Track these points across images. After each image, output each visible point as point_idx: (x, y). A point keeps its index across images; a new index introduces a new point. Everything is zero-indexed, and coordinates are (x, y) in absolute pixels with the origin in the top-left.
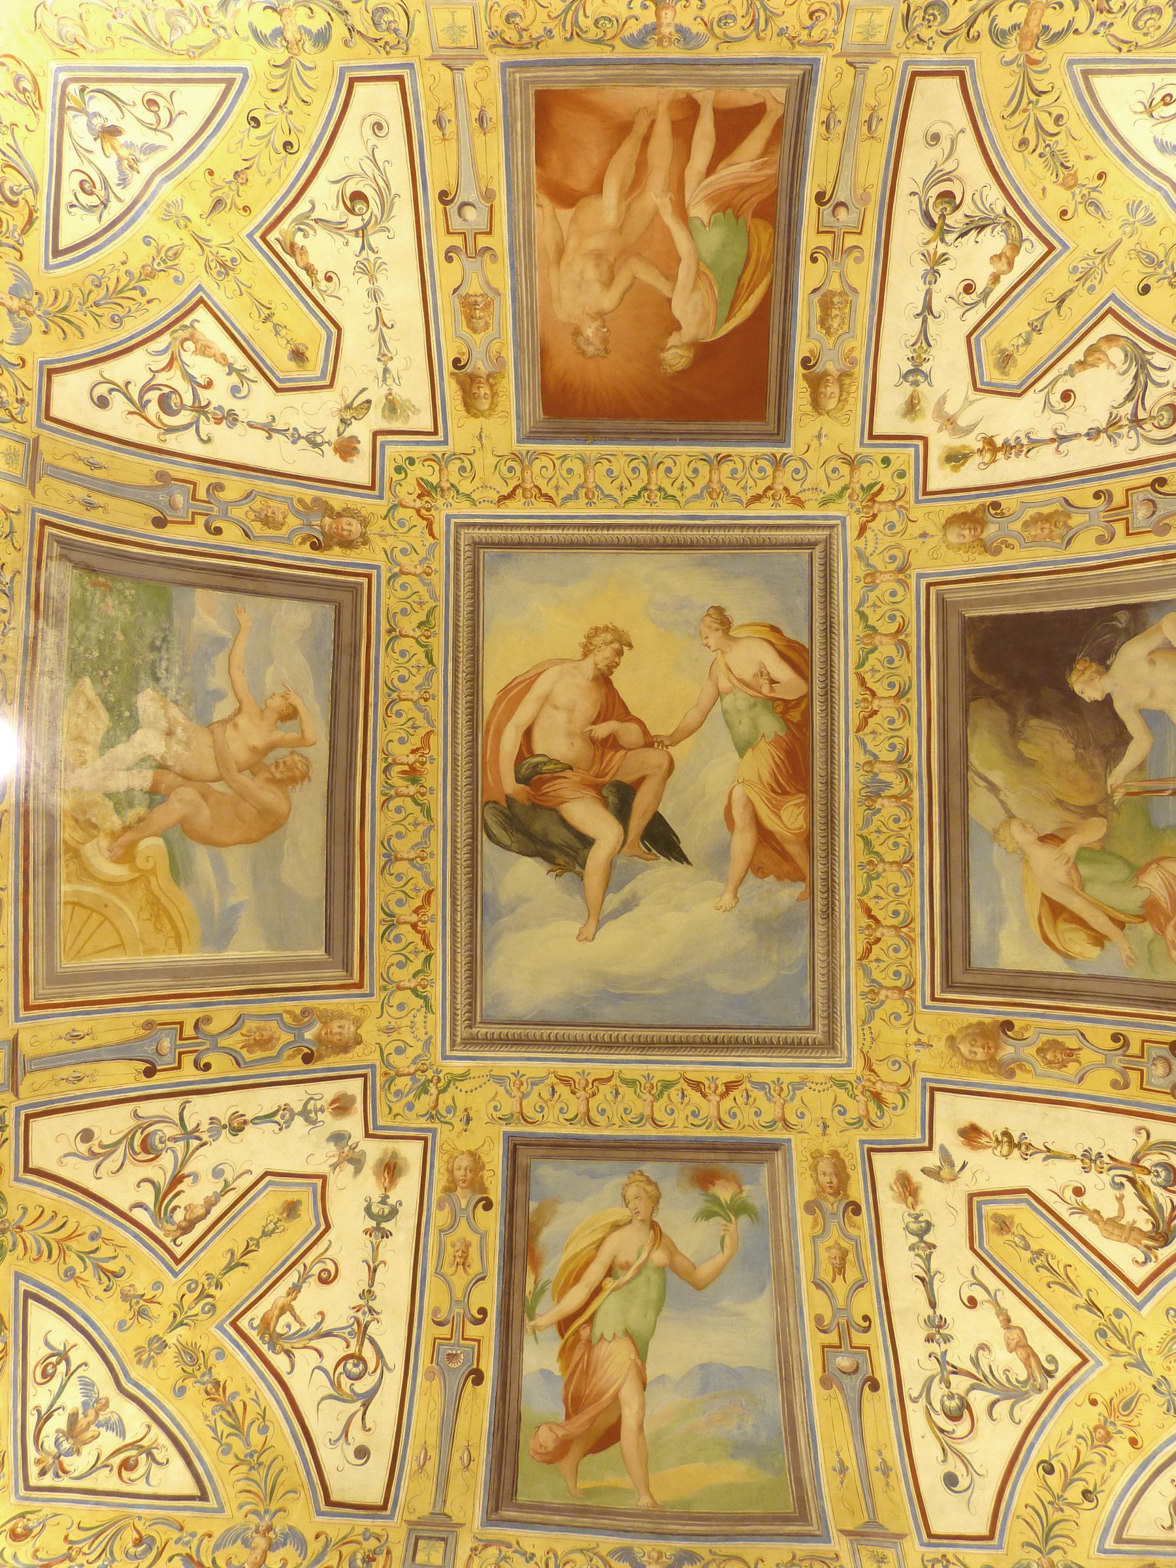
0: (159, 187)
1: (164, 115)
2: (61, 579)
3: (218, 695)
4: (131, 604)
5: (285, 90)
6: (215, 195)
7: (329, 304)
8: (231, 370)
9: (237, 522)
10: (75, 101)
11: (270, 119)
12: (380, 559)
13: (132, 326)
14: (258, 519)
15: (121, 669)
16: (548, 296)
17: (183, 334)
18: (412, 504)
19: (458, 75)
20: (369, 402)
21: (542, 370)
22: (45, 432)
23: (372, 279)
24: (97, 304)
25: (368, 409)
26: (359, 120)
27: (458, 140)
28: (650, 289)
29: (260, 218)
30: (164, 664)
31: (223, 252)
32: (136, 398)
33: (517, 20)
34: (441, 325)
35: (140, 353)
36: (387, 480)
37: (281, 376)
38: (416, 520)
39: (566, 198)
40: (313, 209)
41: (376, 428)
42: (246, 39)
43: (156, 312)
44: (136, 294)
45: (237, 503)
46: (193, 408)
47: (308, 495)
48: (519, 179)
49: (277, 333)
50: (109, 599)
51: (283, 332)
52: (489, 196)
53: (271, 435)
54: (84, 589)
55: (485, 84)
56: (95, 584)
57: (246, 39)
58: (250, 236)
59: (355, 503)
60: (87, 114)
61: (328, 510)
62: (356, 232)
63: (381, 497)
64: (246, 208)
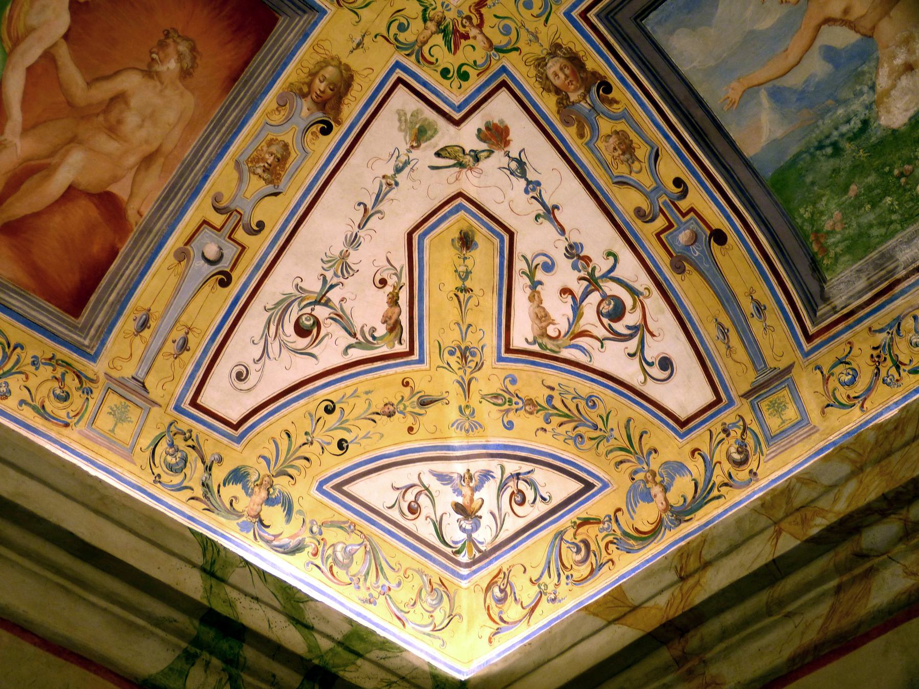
0: (462, 448)
1: (410, 496)
2: (846, 284)
3: (830, 54)
4: (814, 204)
5: (298, 454)
6: (422, 411)
7: (401, 260)
8: (535, 285)
9: (654, 173)
10: (470, 552)
11: (328, 439)
12: (558, 19)
13: (585, 388)
14: (634, 158)
15: (884, 165)
16: (191, 126)
17: (550, 344)
18: (480, 37)
19: (141, 376)
20: (438, 154)
21: (246, 63)
22: (733, 394)
23: (344, 256)
24: (595, 427)
25: (442, 149)
26: (254, 391)
27: (177, 321)
28: (81, 64)
29: (399, 369)
30: (844, 129)
31: (455, 366)
32: (635, 342)
33: (58, 391)
34: (314, 173)
35: (597, 364)
36: (484, 78)
37: (497, 241)
38: (489, 20)
39: (109, 205)
40: (350, 346)
41: (452, 128)
42: (300, 512)
43: (554, 377)
44: (557, 402)
45: (638, 187)
46: (598, 288)
47: (569, 134)
48: (143, 251)
49: (468, 273)
50: (828, 227)
51: (462, 269)
52: (182, 255)
53: (556, 211)
54: (837, 258)
55: (121, 353)
56: (825, 250)
57: (300, 512)
58: (421, 361)
59: (533, 88)
60: (470, 536)
61: (564, 104)
62: (327, 304)
63: (504, 69)
64: (406, 384)
